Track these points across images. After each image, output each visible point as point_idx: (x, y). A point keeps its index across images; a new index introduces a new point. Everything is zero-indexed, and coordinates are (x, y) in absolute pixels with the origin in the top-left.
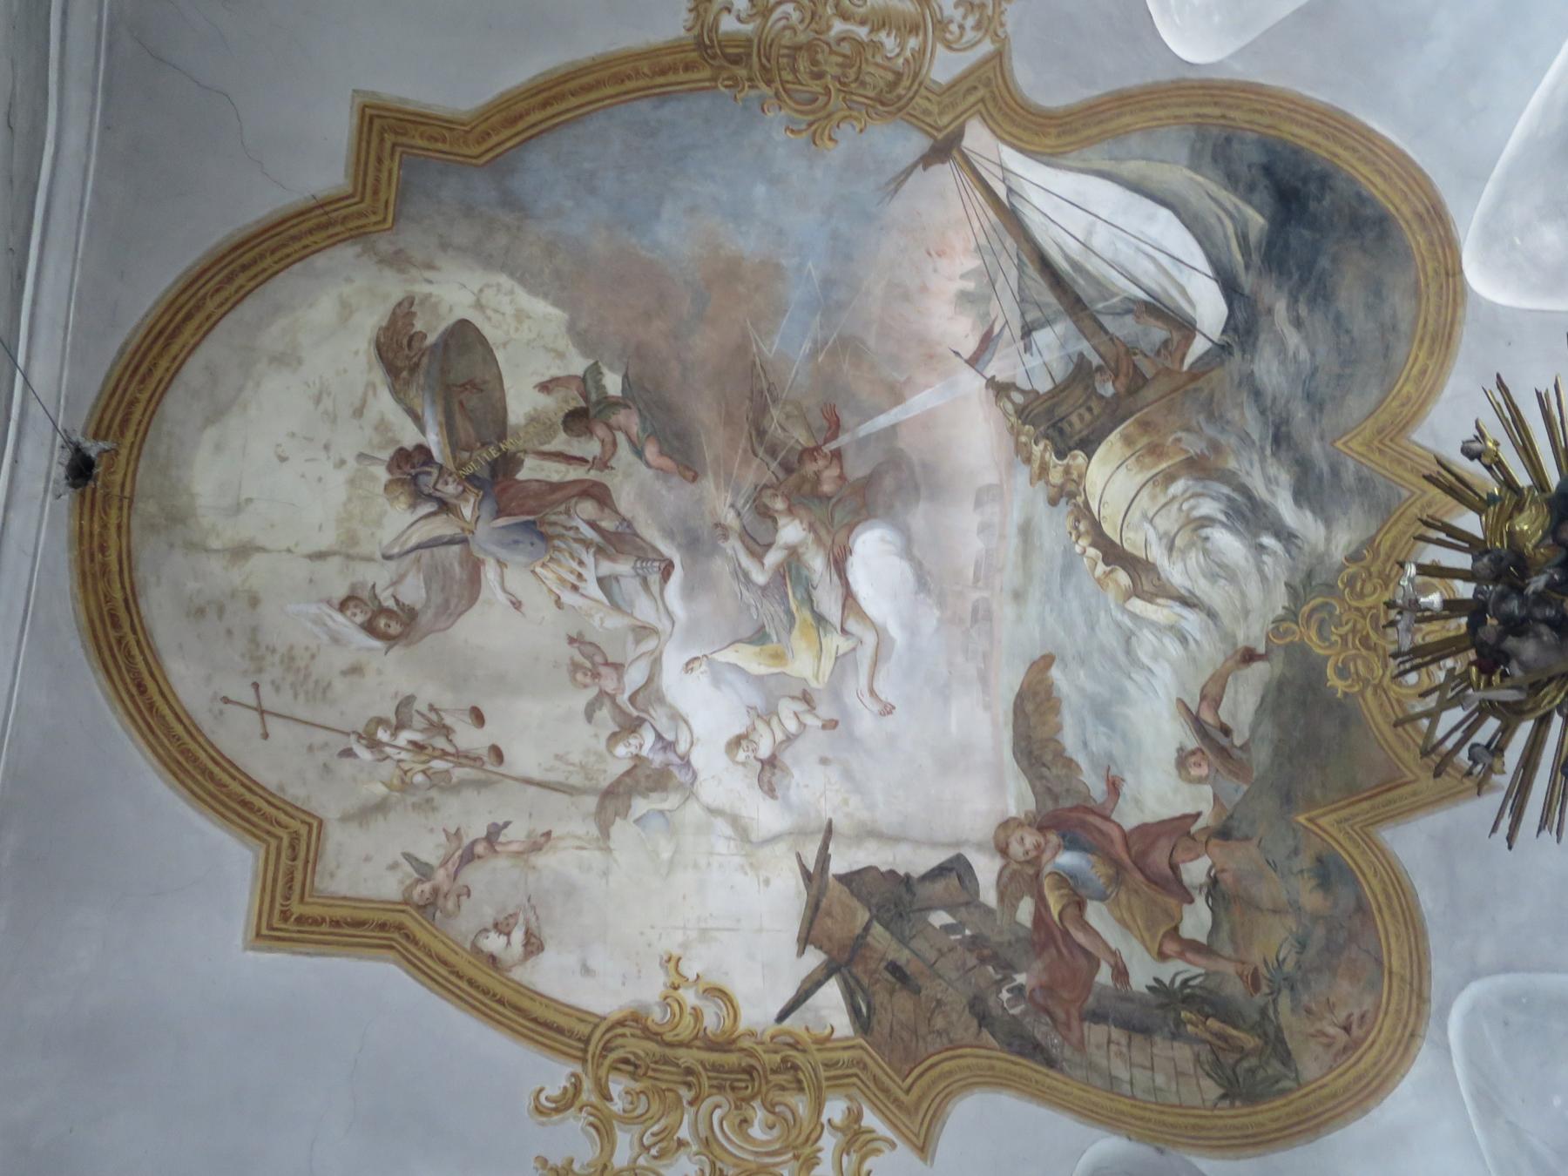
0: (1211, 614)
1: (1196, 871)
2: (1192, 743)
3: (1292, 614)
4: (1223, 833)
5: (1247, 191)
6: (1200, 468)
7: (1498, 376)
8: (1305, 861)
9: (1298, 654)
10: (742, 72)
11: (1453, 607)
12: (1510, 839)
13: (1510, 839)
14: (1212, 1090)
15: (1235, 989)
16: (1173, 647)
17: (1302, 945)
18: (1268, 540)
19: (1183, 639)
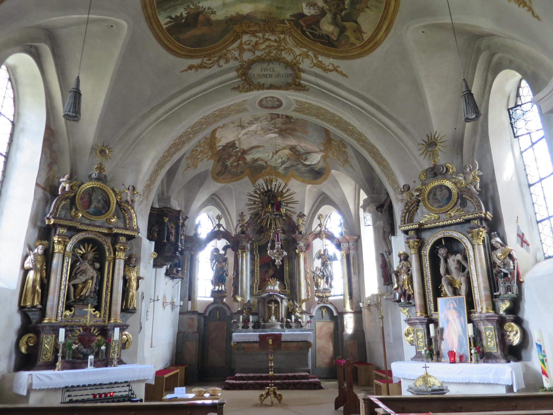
0: (271, 159)
1: (240, 162)
2: (255, 159)
3: (271, 166)
4: (245, 163)
5: (320, 169)
6: (289, 159)
7: (347, 77)
8: (243, 170)
9: (267, 167)
10: (328, 141)
11: (271, 188)
12: (247, 195)
13: (247, 195)
14: (217, 172)
15: (228, 169)
16: (267, 156)
17: (234, 172)
18: (280, 164)
19: (268, 157)
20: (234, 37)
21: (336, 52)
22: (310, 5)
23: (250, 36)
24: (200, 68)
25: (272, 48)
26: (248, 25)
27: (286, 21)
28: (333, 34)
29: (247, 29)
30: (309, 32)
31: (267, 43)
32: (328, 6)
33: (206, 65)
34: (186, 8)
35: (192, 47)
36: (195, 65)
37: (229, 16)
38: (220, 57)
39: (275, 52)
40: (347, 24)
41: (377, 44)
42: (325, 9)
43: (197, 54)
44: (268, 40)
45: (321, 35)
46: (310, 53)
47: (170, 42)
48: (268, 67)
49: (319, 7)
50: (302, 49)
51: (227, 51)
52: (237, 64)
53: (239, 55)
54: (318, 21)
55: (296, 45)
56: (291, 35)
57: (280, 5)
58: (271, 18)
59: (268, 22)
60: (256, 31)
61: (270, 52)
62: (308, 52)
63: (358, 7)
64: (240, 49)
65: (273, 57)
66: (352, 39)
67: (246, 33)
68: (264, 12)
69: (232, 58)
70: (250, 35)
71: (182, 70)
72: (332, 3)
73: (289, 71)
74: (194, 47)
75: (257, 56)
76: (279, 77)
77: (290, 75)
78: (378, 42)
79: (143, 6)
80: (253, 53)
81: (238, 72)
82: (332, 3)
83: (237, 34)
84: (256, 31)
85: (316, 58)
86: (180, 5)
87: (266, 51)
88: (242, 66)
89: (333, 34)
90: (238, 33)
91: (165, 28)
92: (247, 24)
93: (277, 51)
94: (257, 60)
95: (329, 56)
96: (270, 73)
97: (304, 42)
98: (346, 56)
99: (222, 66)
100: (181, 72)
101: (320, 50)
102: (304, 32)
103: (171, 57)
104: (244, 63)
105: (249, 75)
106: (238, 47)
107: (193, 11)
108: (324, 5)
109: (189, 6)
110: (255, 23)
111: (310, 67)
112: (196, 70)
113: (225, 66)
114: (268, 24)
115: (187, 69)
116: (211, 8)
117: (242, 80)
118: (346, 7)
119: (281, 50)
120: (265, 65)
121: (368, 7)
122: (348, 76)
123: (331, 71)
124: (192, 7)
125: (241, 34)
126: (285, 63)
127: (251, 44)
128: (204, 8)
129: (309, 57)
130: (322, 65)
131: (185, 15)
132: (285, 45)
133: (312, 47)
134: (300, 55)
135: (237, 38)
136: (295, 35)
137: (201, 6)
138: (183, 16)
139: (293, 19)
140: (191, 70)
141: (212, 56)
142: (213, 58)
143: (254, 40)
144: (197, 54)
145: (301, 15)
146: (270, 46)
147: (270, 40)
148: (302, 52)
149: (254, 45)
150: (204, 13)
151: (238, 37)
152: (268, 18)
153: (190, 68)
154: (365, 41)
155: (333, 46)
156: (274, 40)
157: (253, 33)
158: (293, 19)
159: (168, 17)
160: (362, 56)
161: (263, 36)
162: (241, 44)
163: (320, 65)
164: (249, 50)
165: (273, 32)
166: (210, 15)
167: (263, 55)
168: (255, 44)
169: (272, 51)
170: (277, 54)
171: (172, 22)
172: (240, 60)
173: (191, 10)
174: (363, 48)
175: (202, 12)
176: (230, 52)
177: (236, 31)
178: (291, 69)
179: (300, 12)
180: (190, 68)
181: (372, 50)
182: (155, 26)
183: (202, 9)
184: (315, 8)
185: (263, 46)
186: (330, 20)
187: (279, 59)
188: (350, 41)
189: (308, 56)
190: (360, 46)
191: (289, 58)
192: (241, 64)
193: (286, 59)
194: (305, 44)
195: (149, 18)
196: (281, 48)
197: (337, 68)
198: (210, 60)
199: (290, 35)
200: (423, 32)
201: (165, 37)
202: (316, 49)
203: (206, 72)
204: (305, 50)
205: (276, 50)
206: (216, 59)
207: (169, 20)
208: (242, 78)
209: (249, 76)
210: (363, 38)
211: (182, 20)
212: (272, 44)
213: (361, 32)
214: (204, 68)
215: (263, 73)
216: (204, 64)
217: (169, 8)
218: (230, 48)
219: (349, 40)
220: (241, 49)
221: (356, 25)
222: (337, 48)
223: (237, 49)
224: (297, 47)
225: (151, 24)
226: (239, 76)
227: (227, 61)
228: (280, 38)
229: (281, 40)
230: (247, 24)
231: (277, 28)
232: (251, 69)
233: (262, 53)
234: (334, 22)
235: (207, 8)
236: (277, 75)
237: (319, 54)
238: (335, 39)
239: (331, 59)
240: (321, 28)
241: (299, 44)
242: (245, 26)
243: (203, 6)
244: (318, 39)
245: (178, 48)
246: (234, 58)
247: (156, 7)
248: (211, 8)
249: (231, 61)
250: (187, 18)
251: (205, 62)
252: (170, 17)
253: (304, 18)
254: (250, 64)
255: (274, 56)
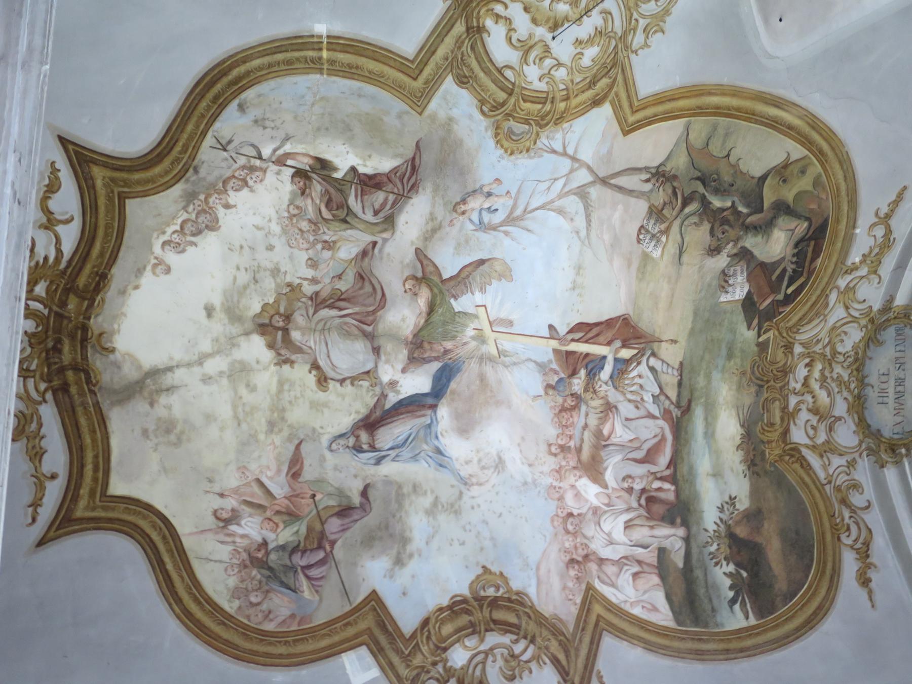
7: (905, 188)
20: (793, 463)
21: (838, 221)
22: (723, 284)
23: (795, 424)
24: (868, 556)
25: (827, 373)
26: (767, 426)
27: (761, 340)
28: (793, 231)
29: (775, 430)
30: (788, 287)
31: (815, 386)
32: (728, 243)
33: (861, 540)
34: (714, 560)
35: (809, 567)
36: (856, 568)
37: (744, 468)
38: (844, 502)
39: (838, 369)
40: (769, 198)
41: (815, 123)
42: (735, 251)
43: (830, 559)
44: (806, 383)
45: (795, 259)
46: (842, 283)
47: (793, 617)
48: (875, 388)
49: (729, 266)
50: (831, 304)
51: (830, 482)
52: (864, 466)
53: (841, 455)
54: (762, 265)
55: (822, 317)
56: (795, 329)
57: (724, 352)
58: (753, 373)
59: (762, 380)
60: (784, 409)
61: (839, 380)
62: (838, 288)
63: (727, 178)
64: (825, 452)
65: (852, 372)
66: (804, 184)
67: (786, 432)
68: (739, 387)
69: (848, 475)
70: (792, 423)
71: (869, 604)
72: (720, 236)
73: (890, 334)
74: (812, 561)
75: (848, 411)
76: (901, 361)
77: (899, 333)
78: (810, 121)
79: (699, 657)
80: (838, 422)
81: (887, 462)
82: (720, 236)
83: (788, 455)
84: (784, 409)
85: (855, 268)
86: (706, 575)
87: (836, 390)
88: (871, 452)
89: (793, 231)
90: (784, 451)
91: (757, 620)
92: (766, 428)
93: (837, 362)
94: (857, 413)
95: (849, 239)
96: (892, 382)
97: (814, 298)
98: (848, 195)
99: (868, 501)
100: (873, 606)
101: (834, 259)
102: (788, 299)
103: (830, 624)
104: (864, 446)
105: (896, 437)
106: (821, 456)
107: (723, 547)
108: (724, 253)
109: (711, 553)
110: (763, 409)
111: (879, 283)
112: (873, 567)
113: (869, 492)
114: (768, 382)
115: (866, 590)
116: (720, 506)
117: (907, 455)
118: (729, 204)
119: (835, 353)
120: (872, 394)
121: (728, 155)
122: (902, 186)
123: (889, 231)
124: (713, 548)
125: (786, 445)
126: (867, 346)
127: (815, 424)
128: (718, 522)
129: (851, 285)
130: (873, 254)
131: (731, 568)
132: (821, 343)
133: (826, 279)
134: (847, 308)
135: (797, 455)
136: (796, 318)
137: (715, 527)
138: (734, 571)
139: (756, 321)
140: (870, 580)
141: (838, 521)
142: (843, 520)
143: (804, 416)
144: (830, 559)
145: (748, 304)
146: (823, 380)
147: (806, 379)
148: (837, 304)
149: (817, 417)
150: (730, 522)
151: (794, 452)
152: (753, 378)
153: (865, 582)
154: (807, 152)
155: (823, 228)
156: (807, 369)
157: (789, 416)
158: (756, 321)
159: (731, 607)
160: (845, 157)
161: (795, 394)
162: (814, 448)
163: (874, 260)
164: (831, 429)
165: (786, 372)
166: (738, 510)
167: (845, 399)
168: (815, 414)
169: (835, 376)
170: (845, 364)
171: (743, 601)
172: (856, 455)
173: (722, 550)
174: (827, 155)
175: (728, 527)
176: (832, 476)
177: (781, 456)
178: (884, 330)
179: (740, 307)
180: (865, 582)
181: (829, 135)
182: (749, 643)
183: (722, 526)
184: (731, 273)
185: (822, 395)
186: (759, 239)
187: (856, 360)
188: (810, 188)
189: (851, 289)
190: (822, 165)
191: (855, 335)
192: (865, 453)
193: (857, 341)
194: (819, 297)
195: (727, 651)
196: (828, 354)
197: (882, 215)
198: (848, 529)
199: (795, 330)
200: (781, 20)
201: (777, 626)
202: (830, 270)
203: (881, 542)
204: (833, 297)
205: (834, 365)
206: (847, 514)
207: (737, 607)
208: (902, 456)
209: (900, 436)
210: (802, 159)
211: (741, 575)
212: (816, 374)
213: (786, 165)
214: (868, 546)
215: (891, 400)
216: (858, 545)
217: (710, 600)
218: (822, 475)
219: (805, 192)
220: (827, 449)
221: (769, 178)
222: (826, 221)
223: (825, 459)
224: (825, 316)
225: (742, 650)
226: (897, 463)
227: (856, 486)
228: (802, 356)
229: (809, 353)
230: (766, 428)
231: (778, 360)
232: (879, 431)
233: (839, 400)
234: (764, 228)
235: (722, 516)
236: (898, 366)
237: (843, 263)
238: (806, 224)
239: (858, 231)
240: (778, 258)
241: (819, 309)
242: (769, 435)
243: (715, 523)
244: (807, 264)
245: (808, 601)
246: (848, 468)
247: (704, 627)
248: (720, 506)
249: (856, 477)
250: (738, 565)
251: (854, 541)
252: (733, 602)
253: (756, 299)
254: (867, 431)
255: (850, 371)
